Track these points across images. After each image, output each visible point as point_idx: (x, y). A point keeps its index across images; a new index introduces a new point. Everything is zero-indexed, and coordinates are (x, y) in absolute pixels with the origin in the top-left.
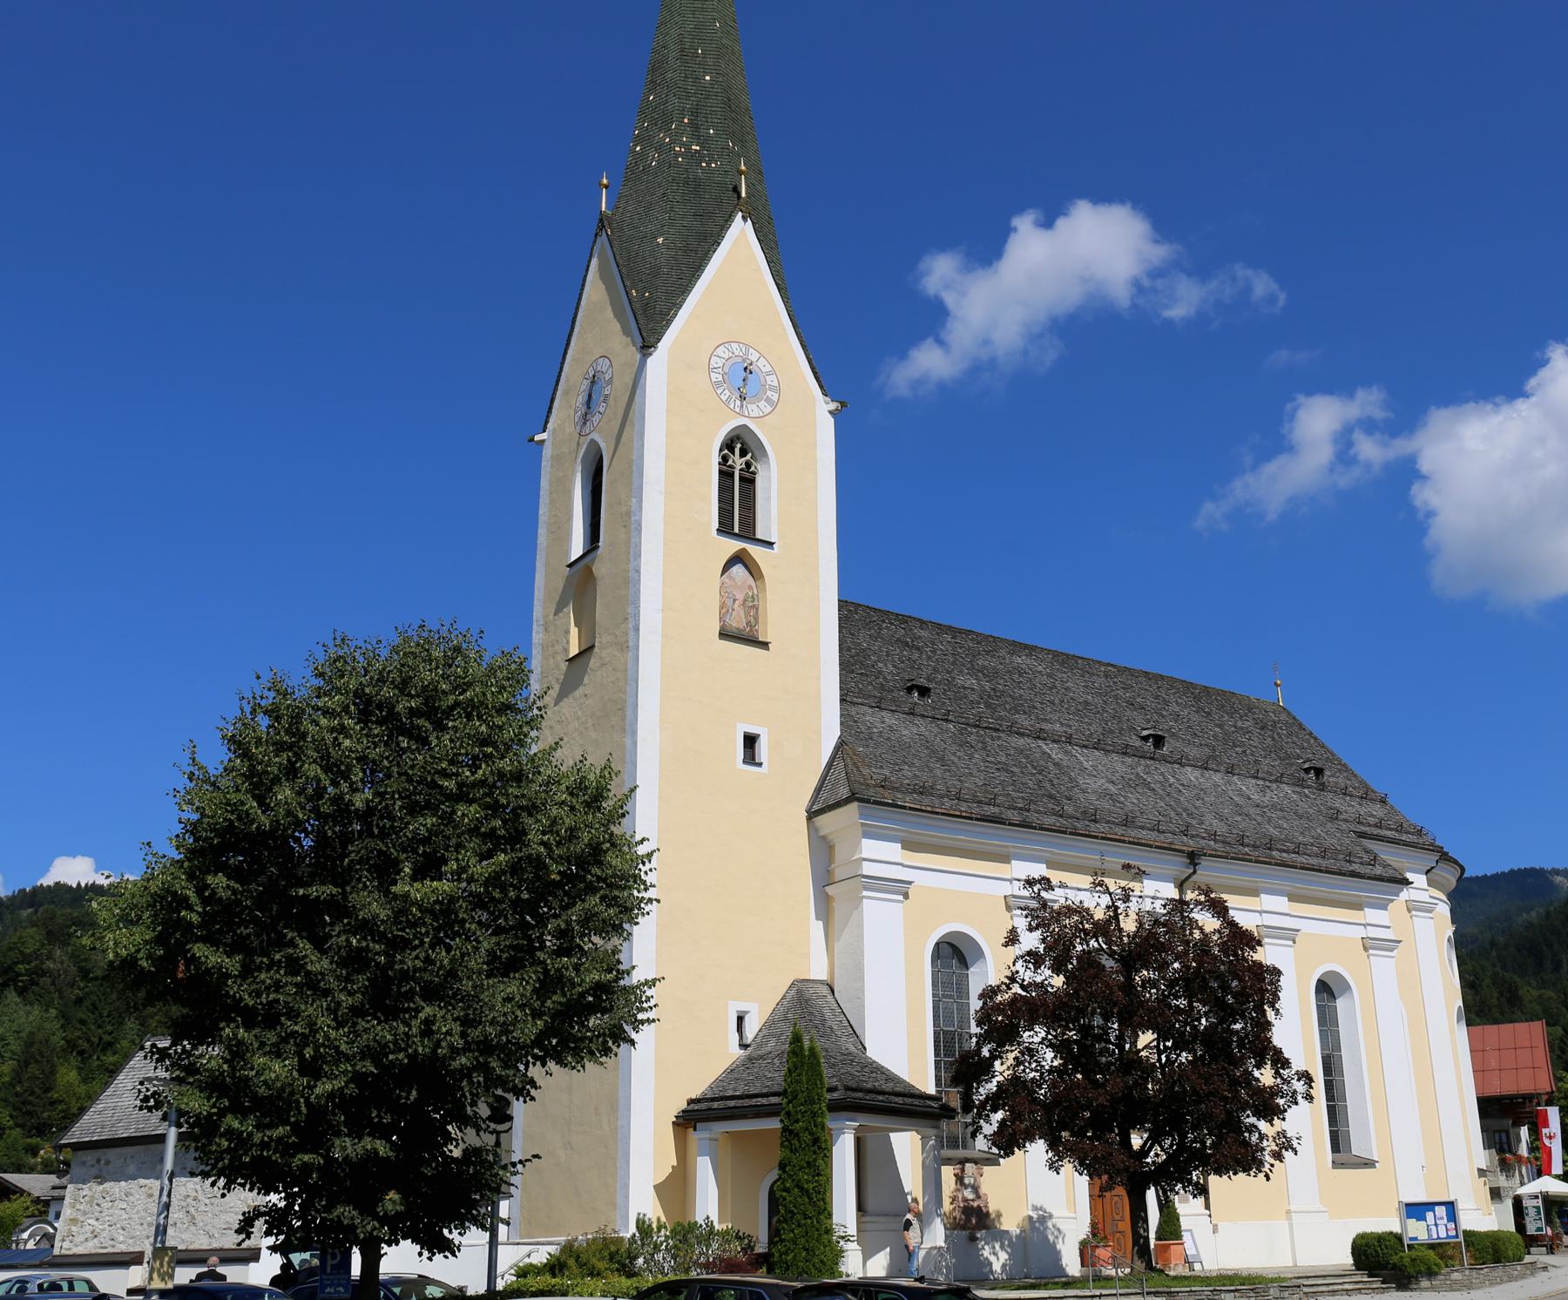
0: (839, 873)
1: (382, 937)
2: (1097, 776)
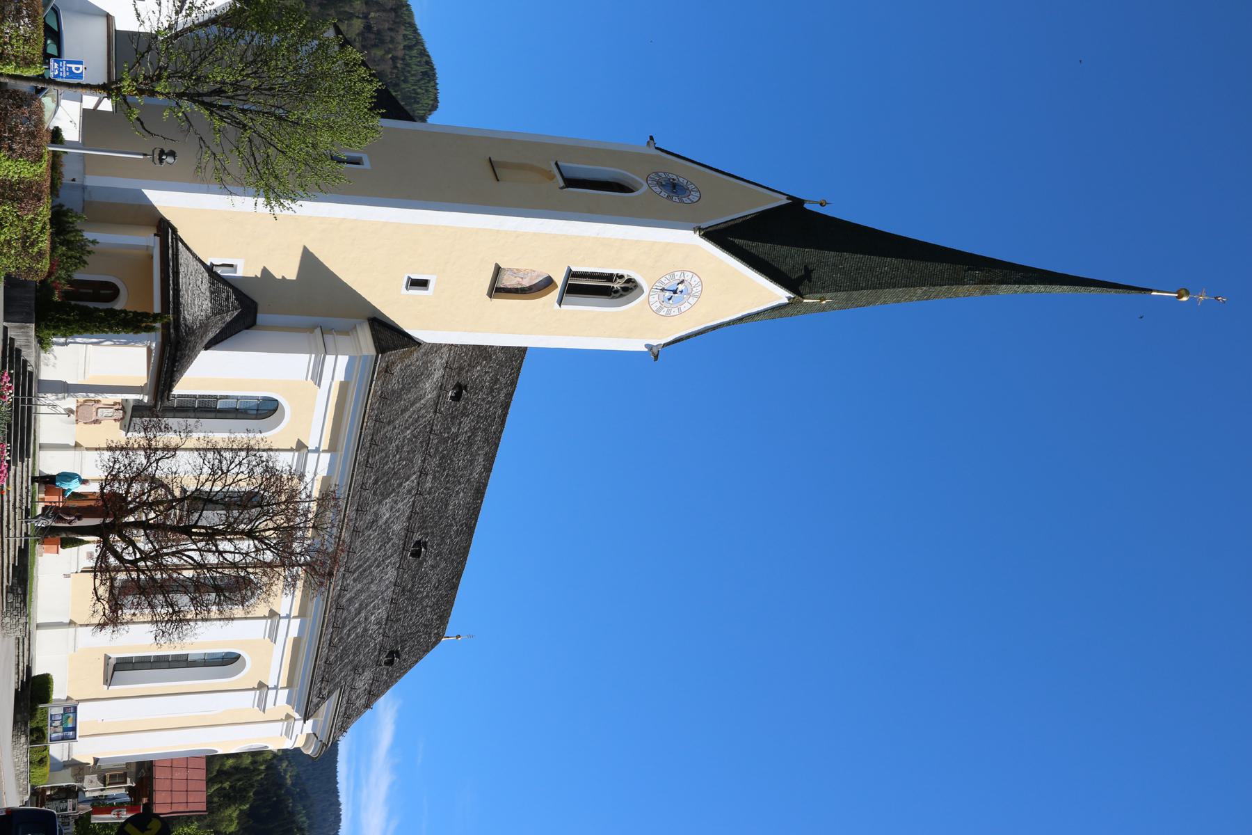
0: (328, 338)
1: (151, 505)
2: (393, 513)
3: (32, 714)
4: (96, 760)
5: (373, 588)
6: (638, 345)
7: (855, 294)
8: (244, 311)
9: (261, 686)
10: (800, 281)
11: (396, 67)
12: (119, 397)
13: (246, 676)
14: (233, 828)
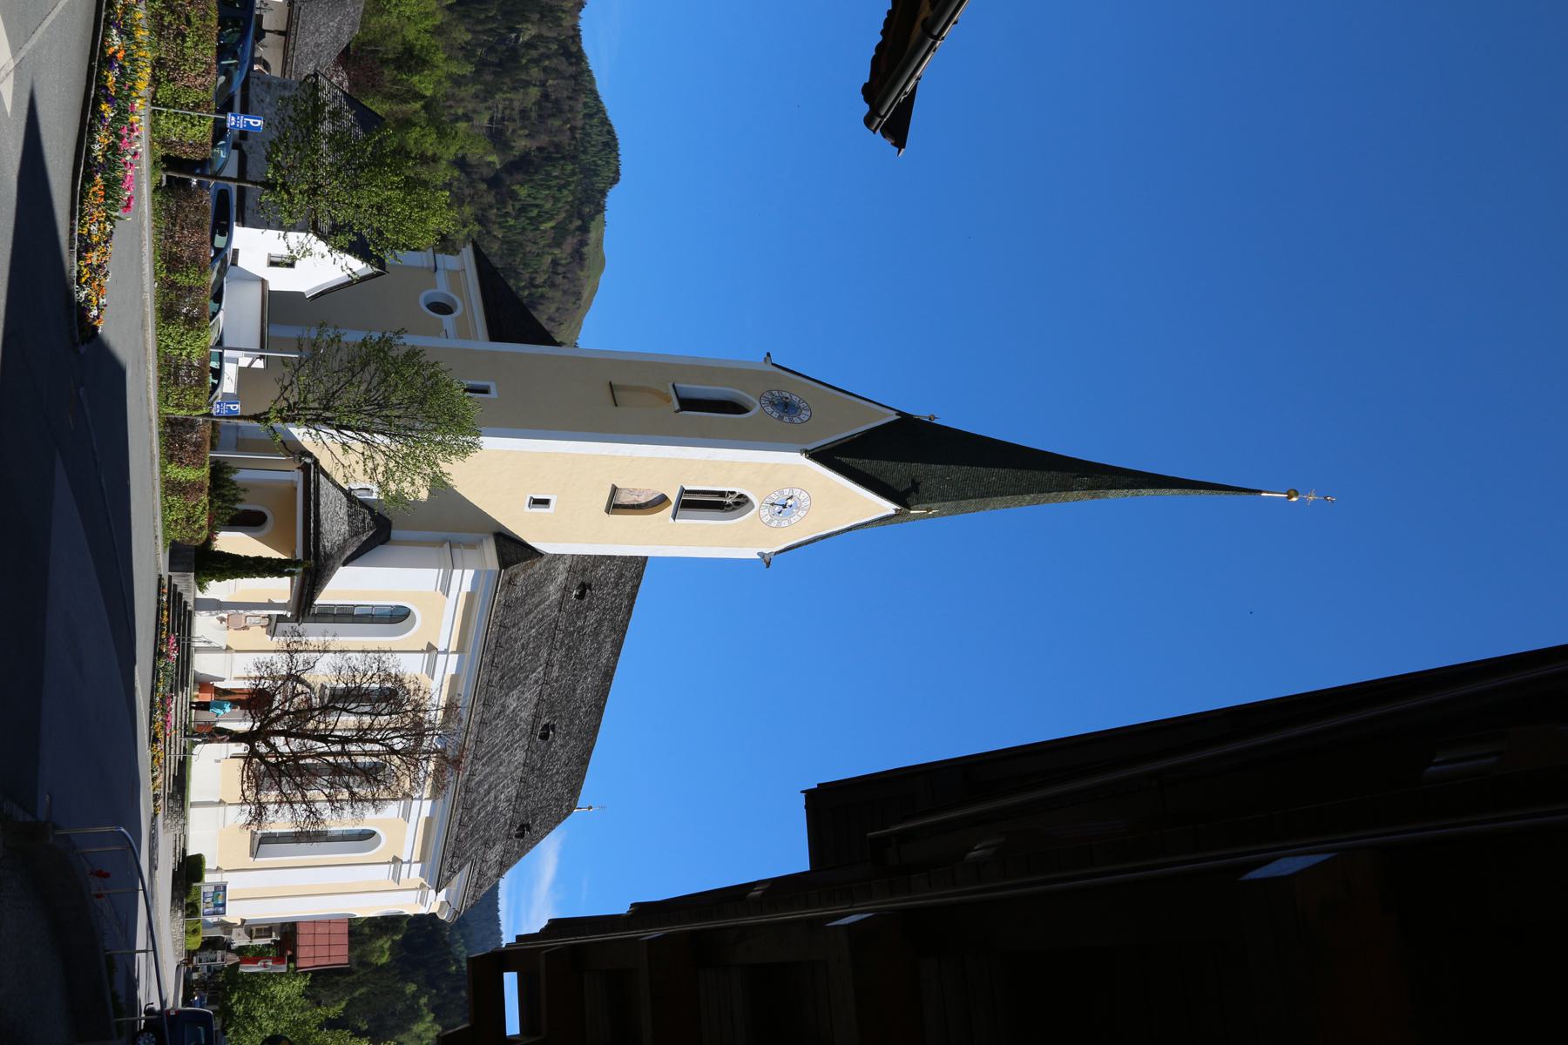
0: (456, 551)
2: (520, 703)
3: (187, 894)
4: (243, 921)
5: (502, 769)
6: (752, 554)
7: (963, 503)
8: (377, 531)
9: (396, 860)
10: (907, 493)
11: (574, 138)
12: (266, 613)
13: (382, 851)
14: (384, 959)
